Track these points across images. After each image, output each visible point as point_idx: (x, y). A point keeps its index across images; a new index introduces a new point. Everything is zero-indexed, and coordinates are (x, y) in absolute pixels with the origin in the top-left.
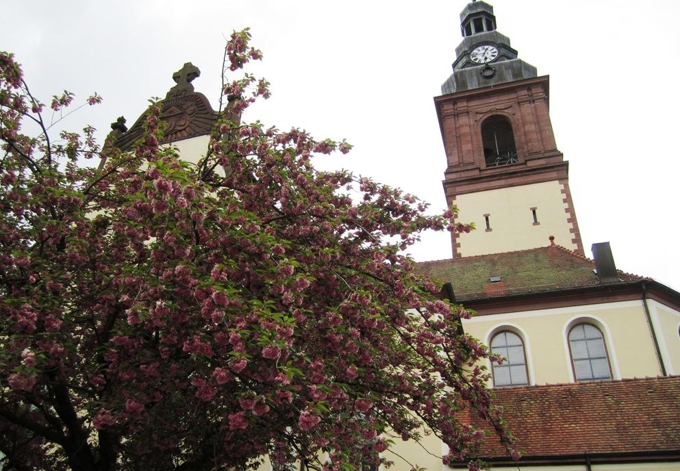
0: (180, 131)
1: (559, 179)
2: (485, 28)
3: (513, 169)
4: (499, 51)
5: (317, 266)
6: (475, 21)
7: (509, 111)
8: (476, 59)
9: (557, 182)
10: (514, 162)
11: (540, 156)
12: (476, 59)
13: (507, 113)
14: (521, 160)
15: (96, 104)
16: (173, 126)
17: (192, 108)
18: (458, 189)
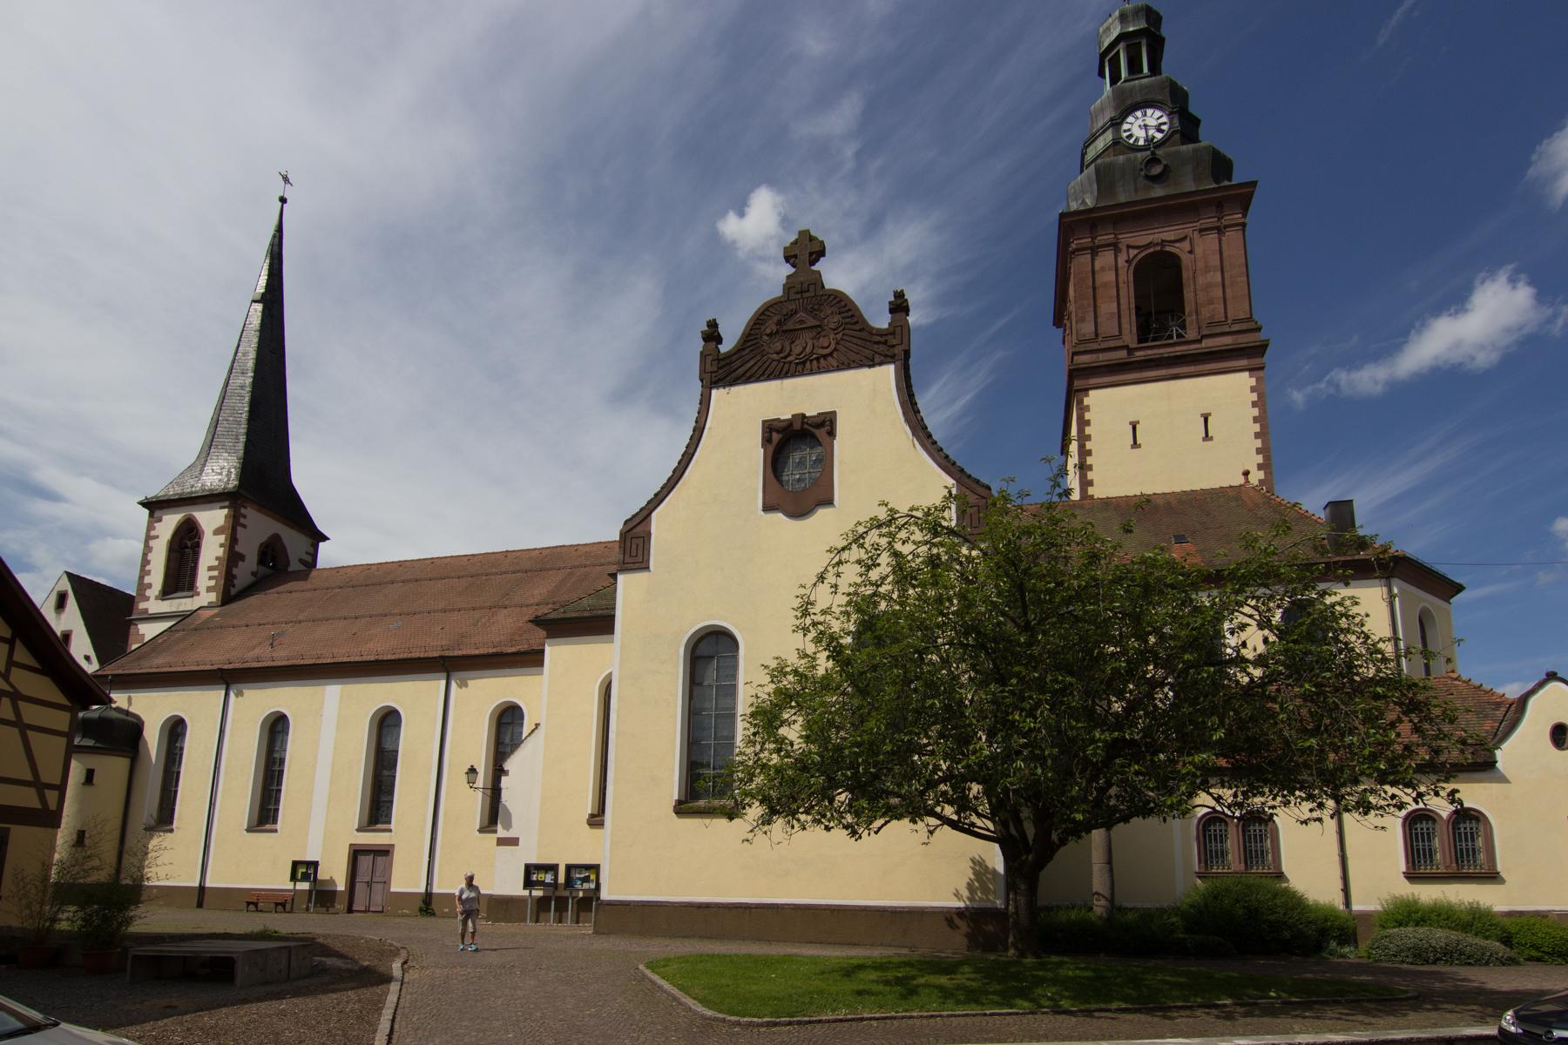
1: (1250, 370)
3: (1208, 344)
7: (1186, 245)
8: (1130, 136)
12: (1130, 136)
13: (1181, 250)
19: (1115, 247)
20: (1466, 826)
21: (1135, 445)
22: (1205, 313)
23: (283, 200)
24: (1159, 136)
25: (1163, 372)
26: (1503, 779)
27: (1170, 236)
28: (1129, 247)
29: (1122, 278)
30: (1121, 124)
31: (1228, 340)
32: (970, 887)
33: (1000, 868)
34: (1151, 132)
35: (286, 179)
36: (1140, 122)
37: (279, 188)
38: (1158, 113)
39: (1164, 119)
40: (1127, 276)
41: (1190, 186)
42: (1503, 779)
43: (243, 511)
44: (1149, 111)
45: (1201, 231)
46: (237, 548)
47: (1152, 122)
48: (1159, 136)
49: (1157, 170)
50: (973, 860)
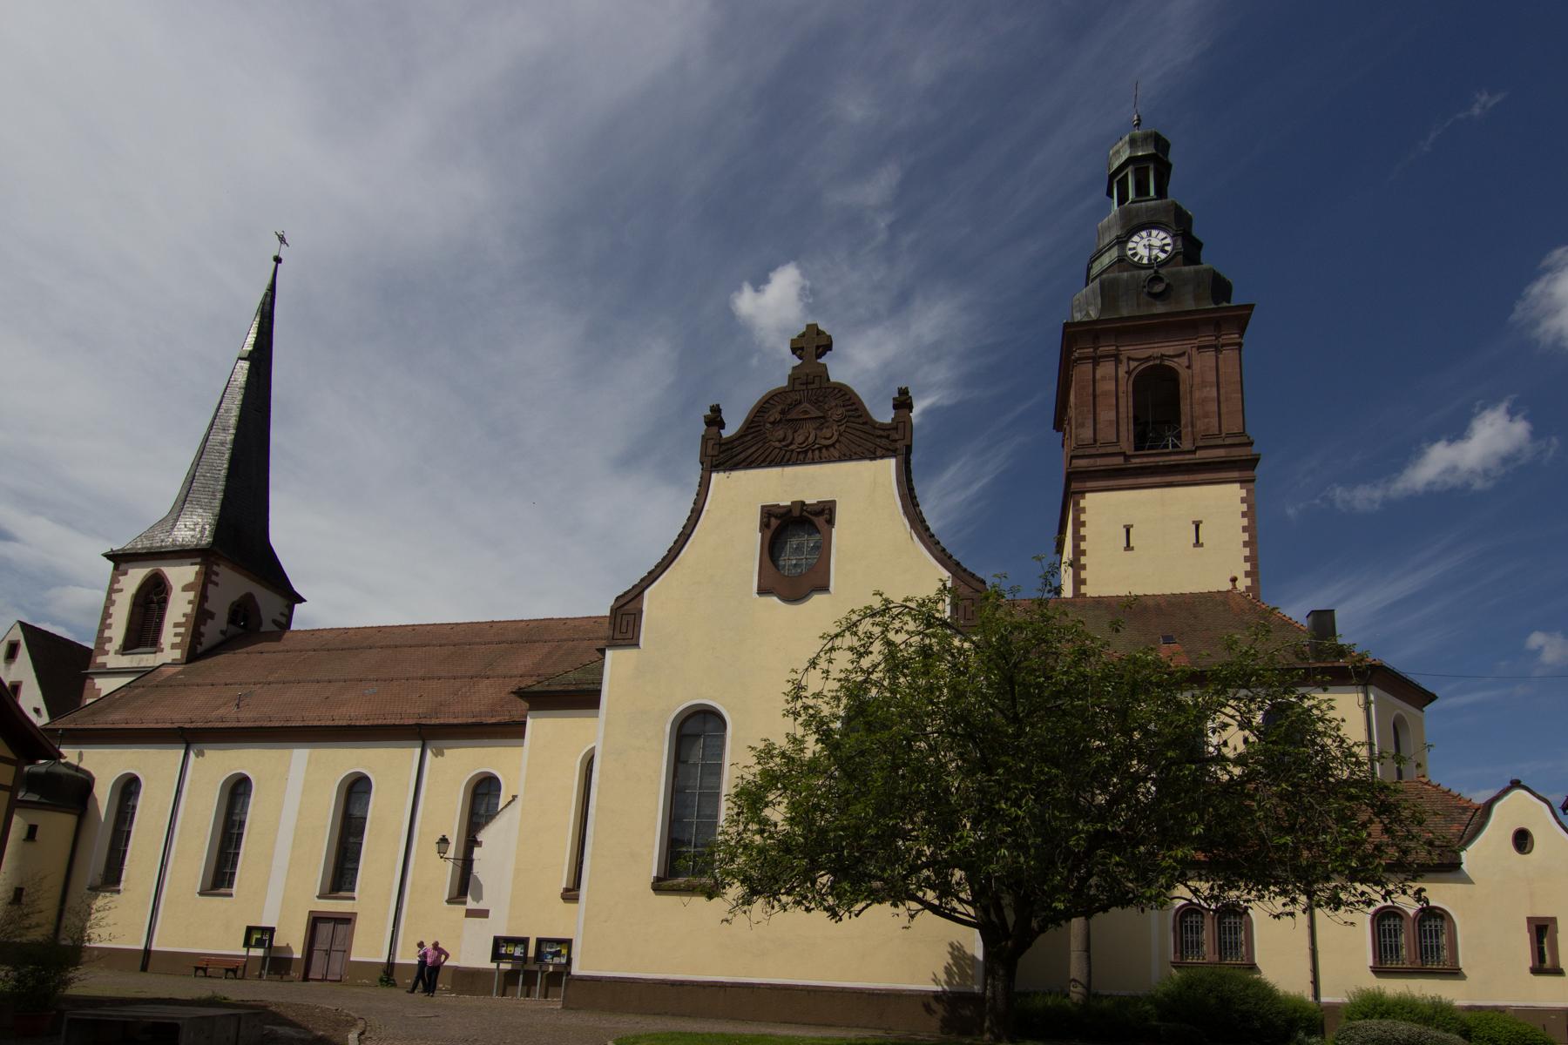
0: (827, 447)
1: (1241, 482)
2: (1152, 193)
4: (1175, 242)
5: (878, 619)
6: (1136, 172)
7: (1184, 361)
8: (1135, 255)
9: (1237, 486)
10: (1175, 446)
11: (1220, 442)
12: (1135, 255)
13: (1179, 364)
14: (1186, 444)
15: (723, 415)
16: (811, 439)
17: (840, 411)
18: (1089, 484)
19: (1117, 358)
20: (1431, 924)
21: (1128, 547)
22: (1200, 425)
23: (278, 260)
24: (1162, 256)
25: (1157, 479)
26: (1467, 880)
27: (1170, 351)
28: (1129, 359)
29: (1122, 388)
30: (1127, 242)
31: (1221, 452)
32: (948, 970)
33: (979, 954)
34: (1155, 252)
35: (282, 239)
36: (1145, 242)
37: (274, 248)
38: (1162, 235)
39: (1168, 241)
40: (1126, 387)
41: (1190, 305)
42: (1467, 880)
43: (215, 568)
44: (1154, 232)
45: (1199, 348)
46: (207, 606)
47: (1156, 242)
48: (1162, 256)
49: (1158, 288)
50: (951, 945)
